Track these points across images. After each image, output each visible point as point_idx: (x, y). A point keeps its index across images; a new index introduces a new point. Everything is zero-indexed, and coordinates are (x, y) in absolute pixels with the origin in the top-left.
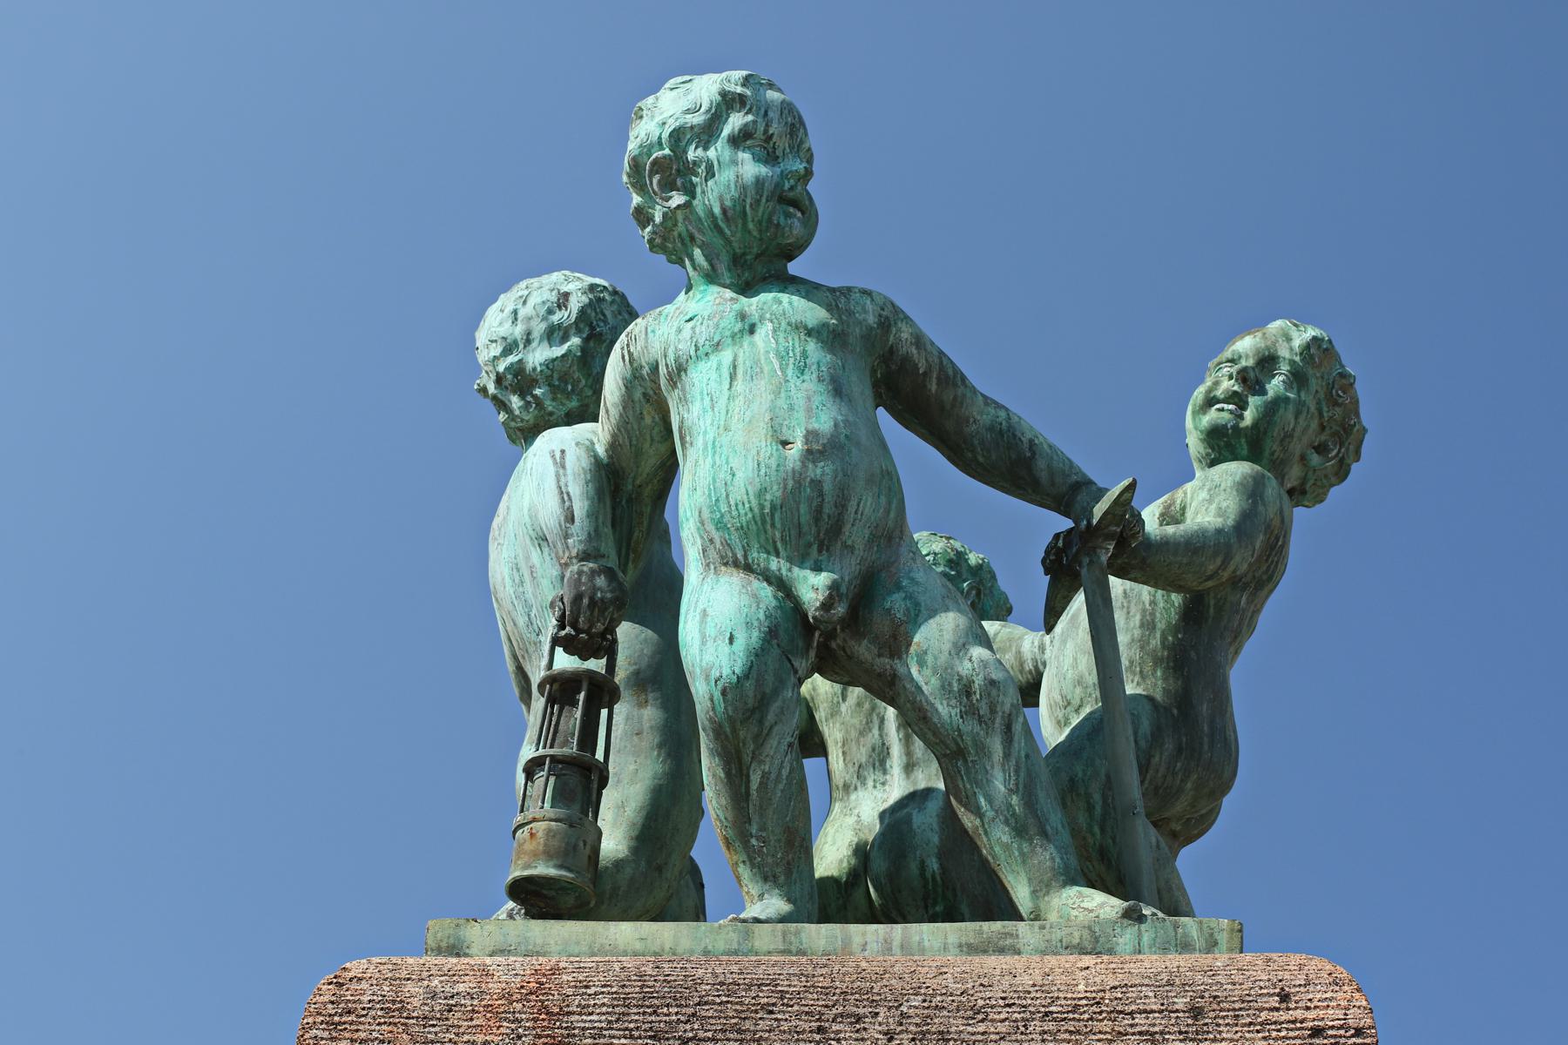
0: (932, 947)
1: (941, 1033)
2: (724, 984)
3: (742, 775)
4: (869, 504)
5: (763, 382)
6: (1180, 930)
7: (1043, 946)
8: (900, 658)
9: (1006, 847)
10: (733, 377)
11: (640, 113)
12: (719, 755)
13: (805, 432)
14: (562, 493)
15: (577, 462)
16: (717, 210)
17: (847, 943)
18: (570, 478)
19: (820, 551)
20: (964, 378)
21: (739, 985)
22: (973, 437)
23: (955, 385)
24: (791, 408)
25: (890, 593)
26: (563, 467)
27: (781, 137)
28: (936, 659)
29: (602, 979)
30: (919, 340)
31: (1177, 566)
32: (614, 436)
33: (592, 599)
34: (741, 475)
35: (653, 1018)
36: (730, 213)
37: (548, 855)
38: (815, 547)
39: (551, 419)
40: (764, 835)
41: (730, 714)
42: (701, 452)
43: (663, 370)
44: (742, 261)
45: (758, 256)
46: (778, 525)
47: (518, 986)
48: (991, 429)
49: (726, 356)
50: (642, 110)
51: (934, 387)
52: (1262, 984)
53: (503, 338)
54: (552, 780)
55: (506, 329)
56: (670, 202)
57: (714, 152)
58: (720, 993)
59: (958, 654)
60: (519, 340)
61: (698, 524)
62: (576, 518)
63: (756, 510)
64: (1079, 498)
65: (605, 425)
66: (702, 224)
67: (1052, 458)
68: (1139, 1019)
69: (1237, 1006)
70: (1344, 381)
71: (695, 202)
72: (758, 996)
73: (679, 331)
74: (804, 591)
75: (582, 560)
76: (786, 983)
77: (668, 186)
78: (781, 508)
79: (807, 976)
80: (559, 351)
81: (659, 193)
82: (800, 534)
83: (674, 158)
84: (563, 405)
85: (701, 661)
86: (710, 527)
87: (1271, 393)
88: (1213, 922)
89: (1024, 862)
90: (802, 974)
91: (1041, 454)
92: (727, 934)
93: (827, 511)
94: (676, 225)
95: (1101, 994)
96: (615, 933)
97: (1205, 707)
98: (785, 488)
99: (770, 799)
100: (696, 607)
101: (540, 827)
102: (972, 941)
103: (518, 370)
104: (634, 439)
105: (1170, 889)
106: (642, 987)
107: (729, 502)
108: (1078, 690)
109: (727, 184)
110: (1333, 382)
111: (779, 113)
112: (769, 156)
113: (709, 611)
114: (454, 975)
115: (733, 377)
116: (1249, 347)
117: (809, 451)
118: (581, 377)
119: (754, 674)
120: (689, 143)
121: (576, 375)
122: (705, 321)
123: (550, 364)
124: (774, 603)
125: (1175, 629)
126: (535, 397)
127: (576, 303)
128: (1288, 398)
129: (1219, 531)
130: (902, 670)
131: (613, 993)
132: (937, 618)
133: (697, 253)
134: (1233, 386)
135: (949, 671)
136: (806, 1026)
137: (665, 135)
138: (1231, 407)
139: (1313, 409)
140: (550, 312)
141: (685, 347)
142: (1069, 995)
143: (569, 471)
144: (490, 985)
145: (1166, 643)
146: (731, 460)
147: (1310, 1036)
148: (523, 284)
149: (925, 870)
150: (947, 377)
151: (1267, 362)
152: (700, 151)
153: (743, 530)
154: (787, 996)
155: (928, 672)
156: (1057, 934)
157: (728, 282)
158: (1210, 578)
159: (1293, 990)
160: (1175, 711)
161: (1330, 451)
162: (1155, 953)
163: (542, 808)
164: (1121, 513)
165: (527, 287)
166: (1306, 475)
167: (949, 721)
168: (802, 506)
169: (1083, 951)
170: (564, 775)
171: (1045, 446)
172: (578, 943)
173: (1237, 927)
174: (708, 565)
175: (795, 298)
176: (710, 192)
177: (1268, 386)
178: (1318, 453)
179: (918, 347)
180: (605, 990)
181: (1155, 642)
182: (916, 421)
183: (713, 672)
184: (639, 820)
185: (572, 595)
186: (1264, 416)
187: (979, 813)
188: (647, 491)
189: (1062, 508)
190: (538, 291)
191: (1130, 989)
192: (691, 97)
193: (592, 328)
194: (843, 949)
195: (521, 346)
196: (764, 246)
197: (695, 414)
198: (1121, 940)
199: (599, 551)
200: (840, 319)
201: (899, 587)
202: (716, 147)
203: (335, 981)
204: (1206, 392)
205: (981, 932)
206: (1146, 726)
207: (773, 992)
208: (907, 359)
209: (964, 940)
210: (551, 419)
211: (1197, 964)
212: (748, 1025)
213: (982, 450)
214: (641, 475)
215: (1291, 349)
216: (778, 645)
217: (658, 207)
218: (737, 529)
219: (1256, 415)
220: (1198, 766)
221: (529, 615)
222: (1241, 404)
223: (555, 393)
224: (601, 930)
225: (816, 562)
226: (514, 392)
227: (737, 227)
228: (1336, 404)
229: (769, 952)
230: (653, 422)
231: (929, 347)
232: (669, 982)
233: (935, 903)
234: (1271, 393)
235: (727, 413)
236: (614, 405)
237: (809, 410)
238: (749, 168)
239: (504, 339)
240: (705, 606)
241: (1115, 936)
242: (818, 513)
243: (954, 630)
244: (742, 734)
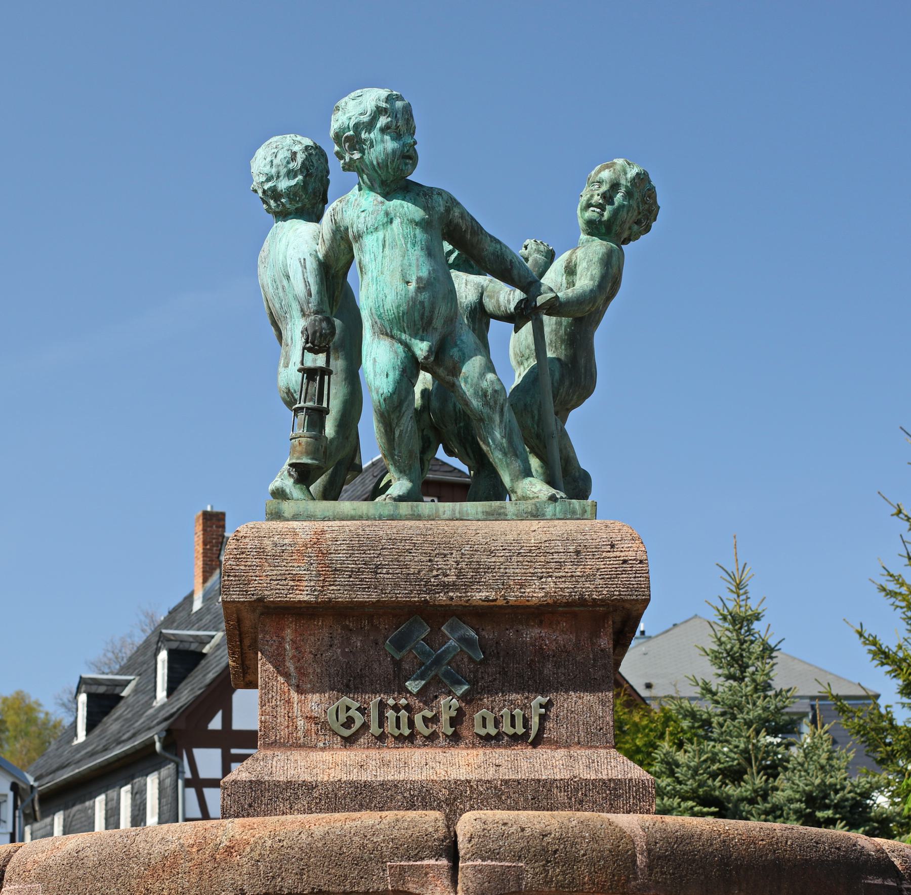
1: (477, 562)
9: (500, 460)
10: (384, 246)
16: (375, 163)
17: (437, 510)
19: (423, 332)
20: (482, 229)
23: (478, 235)
24: (410, 265)
25: (453, 348)
26: (305, 268)
32: (327, 252)
35: (364, 556)
36: (381, 165)
37: (307, 453)
46: (405, 321)
48: (493, 254)
49: (380, 234)
55: (267, 169)
63: (396, 314)
68: (555, 556)
69: (594, 550)
71: (365, 157)
73: (358, 217)
77: (352, 148)
80: (293, 182)
82: (415, 325)
86: (376, 318)
87: (616, 204)
89: (508, 467)
101: (303, 440)
103: (274, 190)
105: (566, 448)
108: (528, 351)
112: (397, 137)
115: (384, 246)
119: (397, 392)
120: (362, 130)
126: (282, 202)
127: (300, 158)
128: (624, 205)
129: (591, 291)
136: (425, 559)
137: (351, 126)
139: (635, 207)
140: (288, 163)
141: (362, 227)
143: (308, 271)
147: (622, 564)
151: (615, 186)
161: (642, 223)
174: (374, 333)
175: (410, 204)
181: (562, 332)
184: (339, 417)
188: (341, 273)
192: (362, 106)
200: (429, 215)
201: (456, 345)
206: (557, 375)
208: (457, 225)
209: (484, 510)
212: (401, 558)
215: (626, 179)
228: (646, 203)
234: (616, 204)
237: (418, 266)
238: (390, 144)
239: (267, 174)
244: (392, 416)
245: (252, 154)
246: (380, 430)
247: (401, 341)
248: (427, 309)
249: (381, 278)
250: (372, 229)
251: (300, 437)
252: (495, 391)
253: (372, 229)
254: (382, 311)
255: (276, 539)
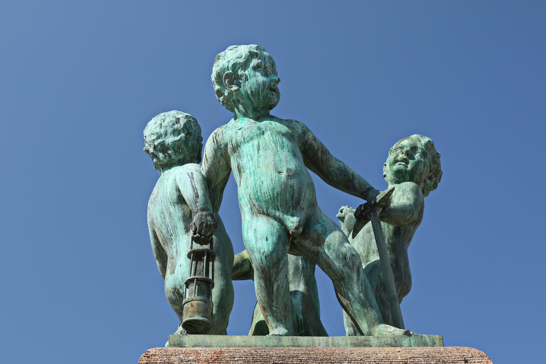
0: (342, 344)
2: (281, 357)
3: (271, 285)
4: (308, 193)
5: (269, 151)
6: (423, 339)
7: (379, 344)
8: (321, 246)
9: (359, 311)
10: (259, 149)
11: (219, 58)
12: (263, 278)
13: (286, 169)
14: (193, 187)
15: (197, 178)
16: (249, 92)
17: (314, 343)
18: (196, 182)
19: (293, 210)
20: (329, 152)
21: (285, 357)
22: (332, 172)
24: (281, 161)
25: (316, 224)
26: (193, 179)
27: (269, 68)
28: (334, 247)
29: (239, 355)
30: (315, 139)
31: (399, 217)
32: (209, 168)
33: (207, 224)
34: (265, 184)
36: (254, 93)
37: (199, 312)
38: (292, 208)
39: (173, 161)
40: (278, 306)
41: (268, 264)
42: (248, 175)
43: (230, 146)
44: (257, 109)
45: (262, 108)
46: (279, 200)
47: (210, 357)
48: (338, 169)
49: (255, 142)
50: (220, 57)
51: (320, 155)
52: (458, 357)
53: (157, 133)
54: (197, 286)
55: (158, 130)
56: (232, 88)
57: (248, 72)
58: (280, 360)
59: (341, 245)
60: (163, 134)
61: (249, 199)
62: (199, 196)
63: (272, 195)
64: (370, 193)
65: (206, 164)
66: (243, 97)
67: (360, 179)
70: (438, 156)
71: (241, 89)
72: (293, 361)
74: (288, 223)
75: (202, 211)
76: (301, 356)
77: (231, 83)
78: (280, 194)
79: (308, 354)
80: (177, 138)
81: (228, 85)
83: (233, 74)
84: (178, 157)
85: (256, 246)
86: (254, 201)
87: (416, 159)
88: (434, 336)
89: (365, 316)
90: (306, 354)
91: (356, 178)
92: (273, 340)
93: (295, 196)
94: (232, 96)
95: (406, 360)
96: (235, 340)
97: (402, 264)
98: (281, 188)
99: (280, 294)
100: (251, 228)
101: (195, 303)
102: (355, 342)
103: (163, 144)
104: (216, 169)
106: (253, 358)
107: (261, 192)
109: (253, 83)
110: (435, 156)
111: (268, 59)
112: (266, 75)
113: (257, 229)
114: (187, 354)
115: (259, 149)
116: (407, 143)
117: (289, 176)
118: (185, 147)
119: (276, 251)
120: (239, 68)
121: (183, 147)
122: (246, 130)
123: (174, 142)
124: (279, 227)
125: (392, 238)
126: (169, 154)
127: (182, 122)
128: (421, 161)
129: (410, 205)
130: (321, 251)
131: (243, 360)
132: (333, 233)
133: (240, 106)
134: (404, 156)
135: (339, 251)
138: (403, 163)
139: (428, 164)
140: (174, 124)
141: (240, 138)
142: (396, 361)
143: (195, 180)
144: (201, 357)
145: (390, 242)
146: (261, 178)
148: (162, 114)
149: (298, 318)
150: (324, 151)
151: (414, 148)
152: (242, 71)
153: (267, 202)
154: (303, 361)
155: (331, 251)
156: (383, 340)
157: (251, 116)
158: (407, 221)
159: (468, 359)
160: (394, 265)
161: (432, 179)
162: (416, 346)
163: (195, 296)
164: (387, 199)
165: (164, 116)
166: (425, 187)
167: (339, 268)
168: (287, 194)
169: (392, 346)
170: (201, 285)
171: (357, 176)
172: (222, 343)
173: (441, 338)
174: (253, 213)
175: (277, 123)
176: (246, 86)
177: (415, 157)
178: (429, 179)
179: (314, 141)
180: (240, 359)
182: (313, 166)
183: (261, 250)
185: (199, 223)
186: (415, 167)
187: (349, 299)
188: (219, 187)
189: (363, 196)
190: (170, 116)
191: (416, 359)
192: (238, 53)
193: (188, 131)
194: (313, 345)
195: (163, 136)
196: (265, 105)
197: (245, 162)
198: (404, 342)
199: (207, 208)
200: (292, 131)
201: (319, 223)
202: (248, 70)
203: (146, 356)
204: (394, 158)
205: (358, 339)
207: (297, 359)
208: (311, 145)
209: (352, 342)
210: (173, 161)
211: (434, 350)
213: (335, 176)
214: (217, 182)
215: (421, 144)
216: (282, 241)
217: (226, 90)
218: (264, 202)
219: (412, 166)
220: (402, 284)
221: (167, 229)
222: (407, 162)
223: (175, 153)
224: (230, 338)
225: (292, 213)
226: (161, 152)
227: (256, 98)
228: (435, 163)
229: (288, 346)
230: (223, 164)
231: (318, 141)
232: (262, 356)
233: (301, 330)
234: (416, 159)
235: (258, 162)
236: (210, 158)
237: (287, 161)
238: (260, 78)
239: (157, 133)
240: (255, 227)
241: (402, 341)
242: (293, 196)
243: (339, 237)
245: (145, 125)
246: (260, 286)
247: (275, 218)
248: (296, 192)
249: (258, 171)
250: (248, 139)
251: (192, 300)
252: (353, 255)
253: (248, 139)
254: (259, 194)
255: (181, 356)
